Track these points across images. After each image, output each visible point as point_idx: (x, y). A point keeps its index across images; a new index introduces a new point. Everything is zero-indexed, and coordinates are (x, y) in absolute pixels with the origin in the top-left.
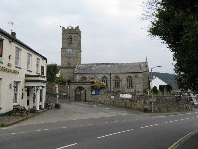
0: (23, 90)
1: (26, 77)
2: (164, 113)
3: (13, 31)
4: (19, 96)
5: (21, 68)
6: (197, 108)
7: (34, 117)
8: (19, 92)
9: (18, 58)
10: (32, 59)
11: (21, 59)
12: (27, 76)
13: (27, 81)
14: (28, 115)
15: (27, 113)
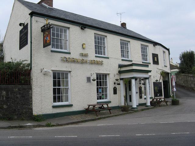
0: (115, 83)
1: (119, 67)
2: (102, 50)
3: (122, 22)
4: (110, 91)
5: (108, 58)
6: (192, 90)
7: (121, 117)
8: (108, 86)
9: (128, 51)
10: (131, 45)
11: (107, 47)
12: (120, 66)
13: (120, 72)
14: (111, 114)
15: (110, 111)
